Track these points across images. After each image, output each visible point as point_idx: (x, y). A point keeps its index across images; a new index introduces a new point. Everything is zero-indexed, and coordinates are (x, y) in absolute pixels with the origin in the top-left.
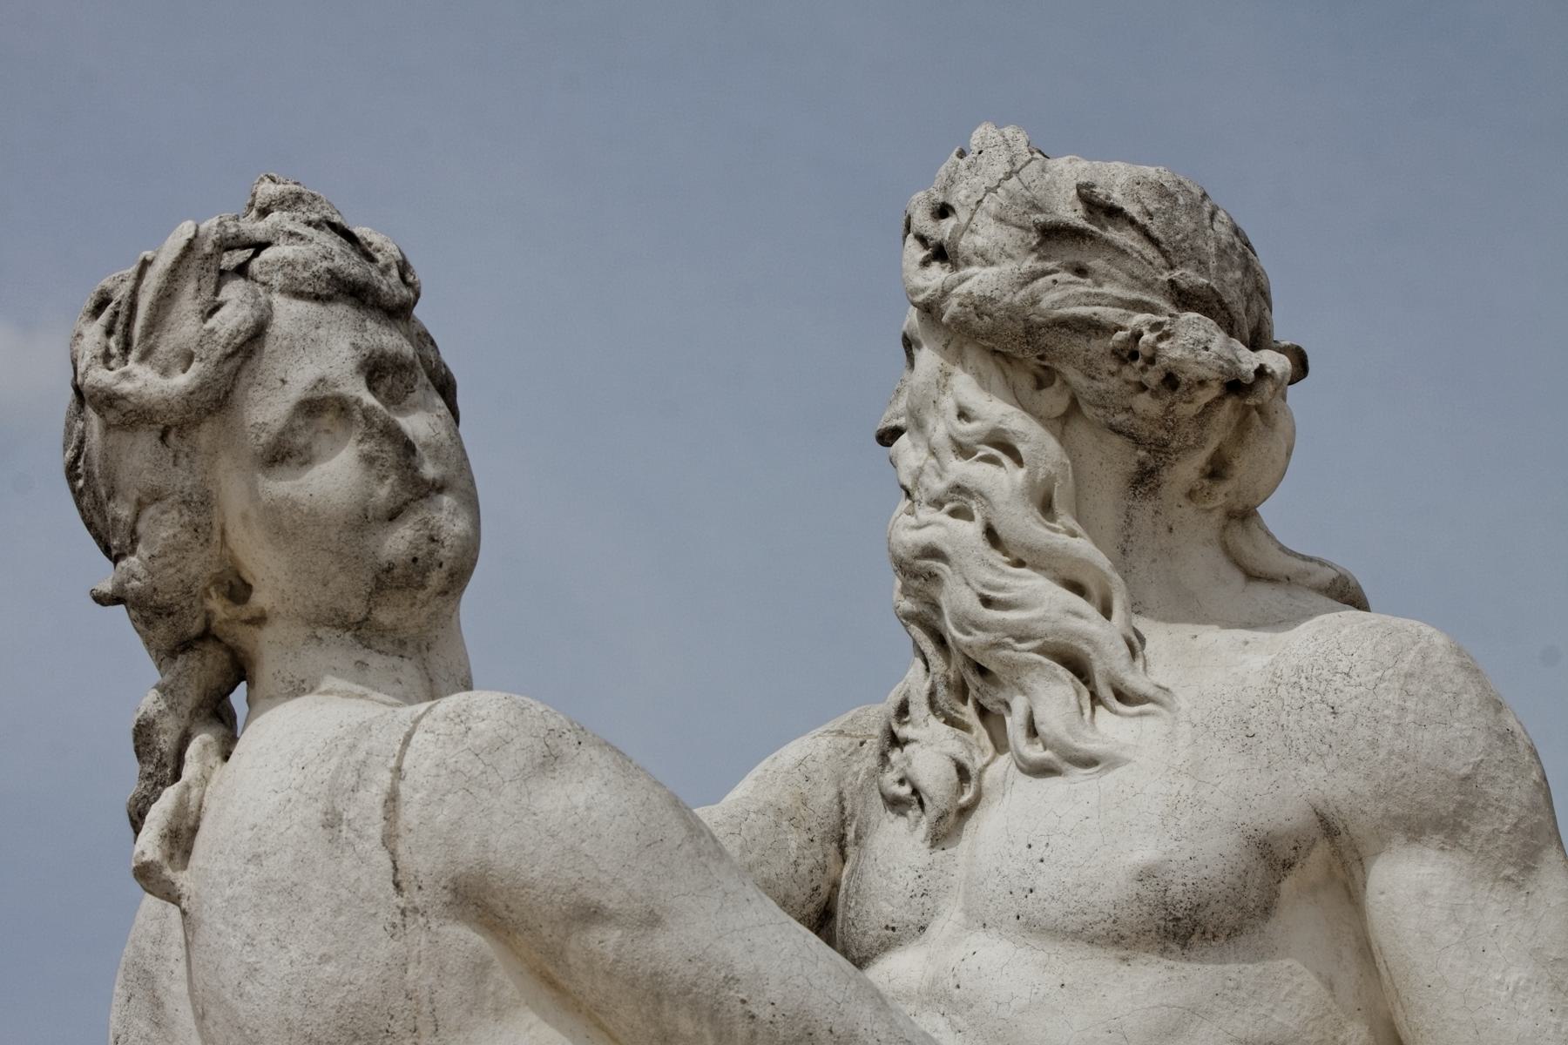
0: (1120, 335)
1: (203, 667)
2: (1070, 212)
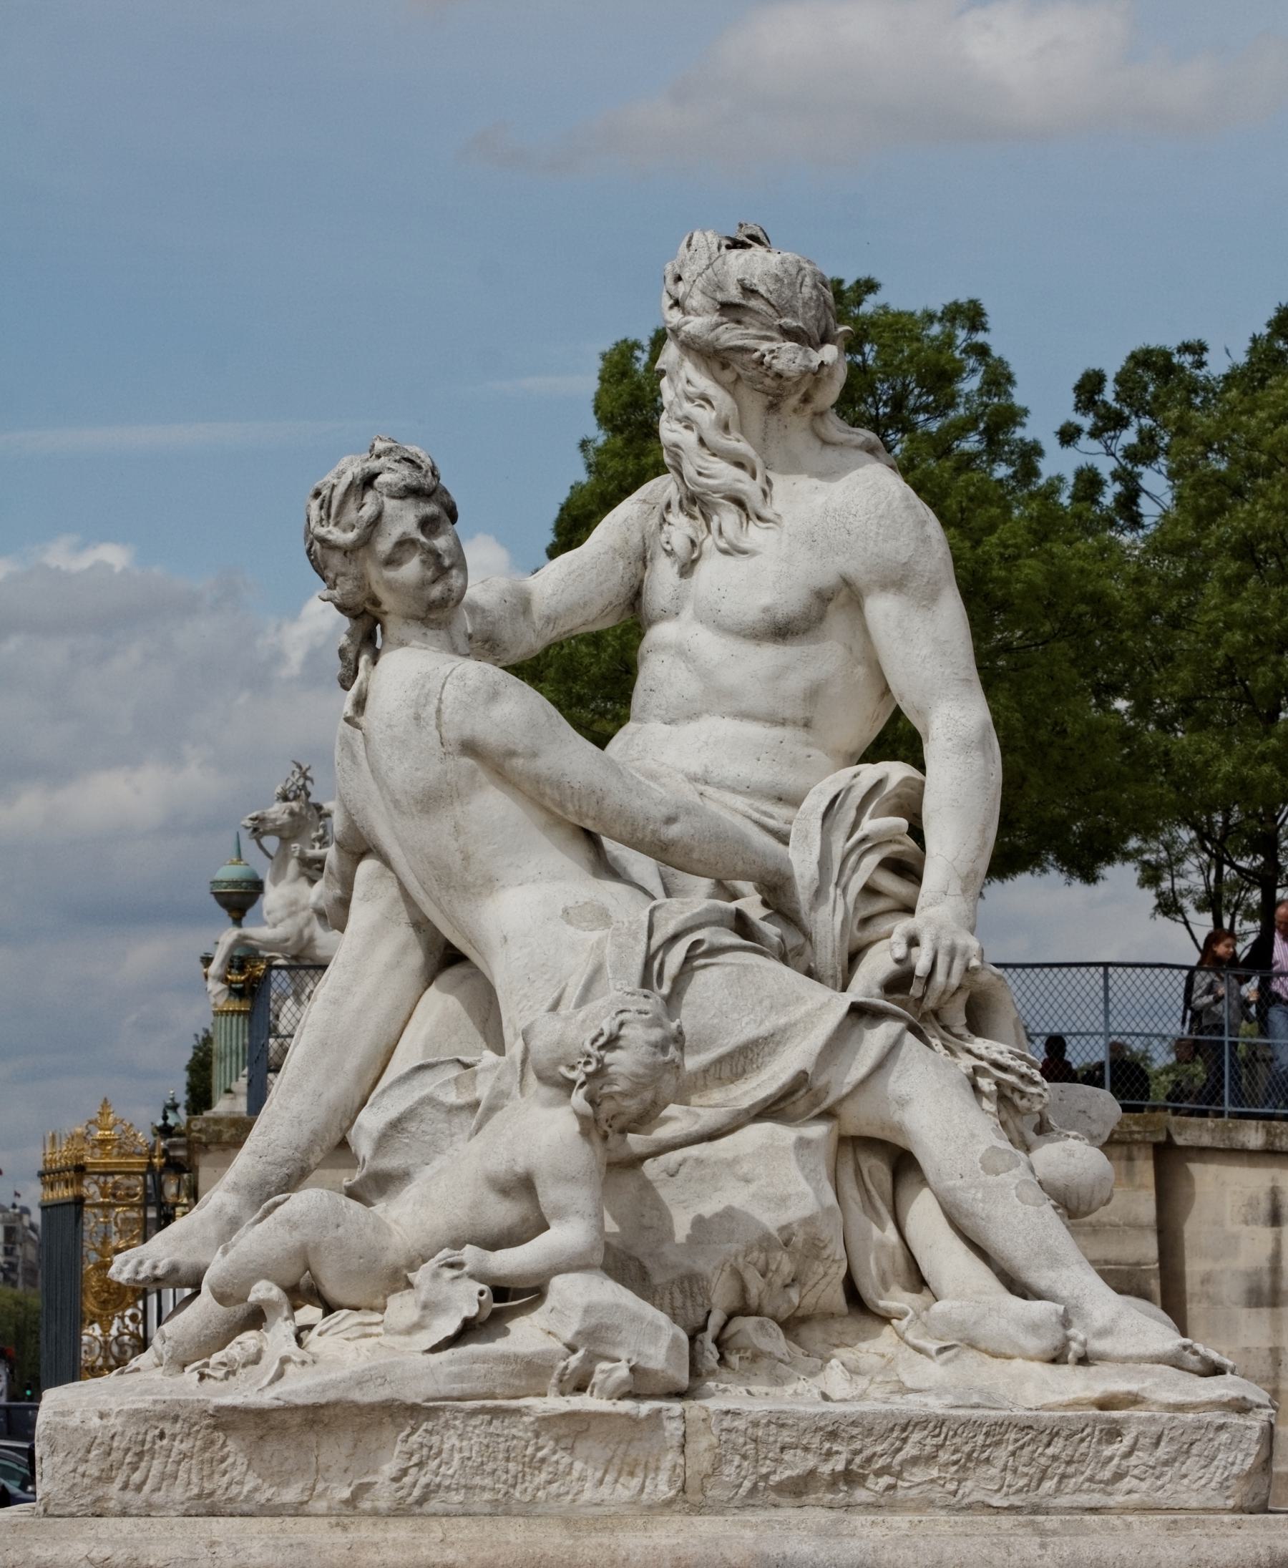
1: (364, 624)
2: (734, 294)
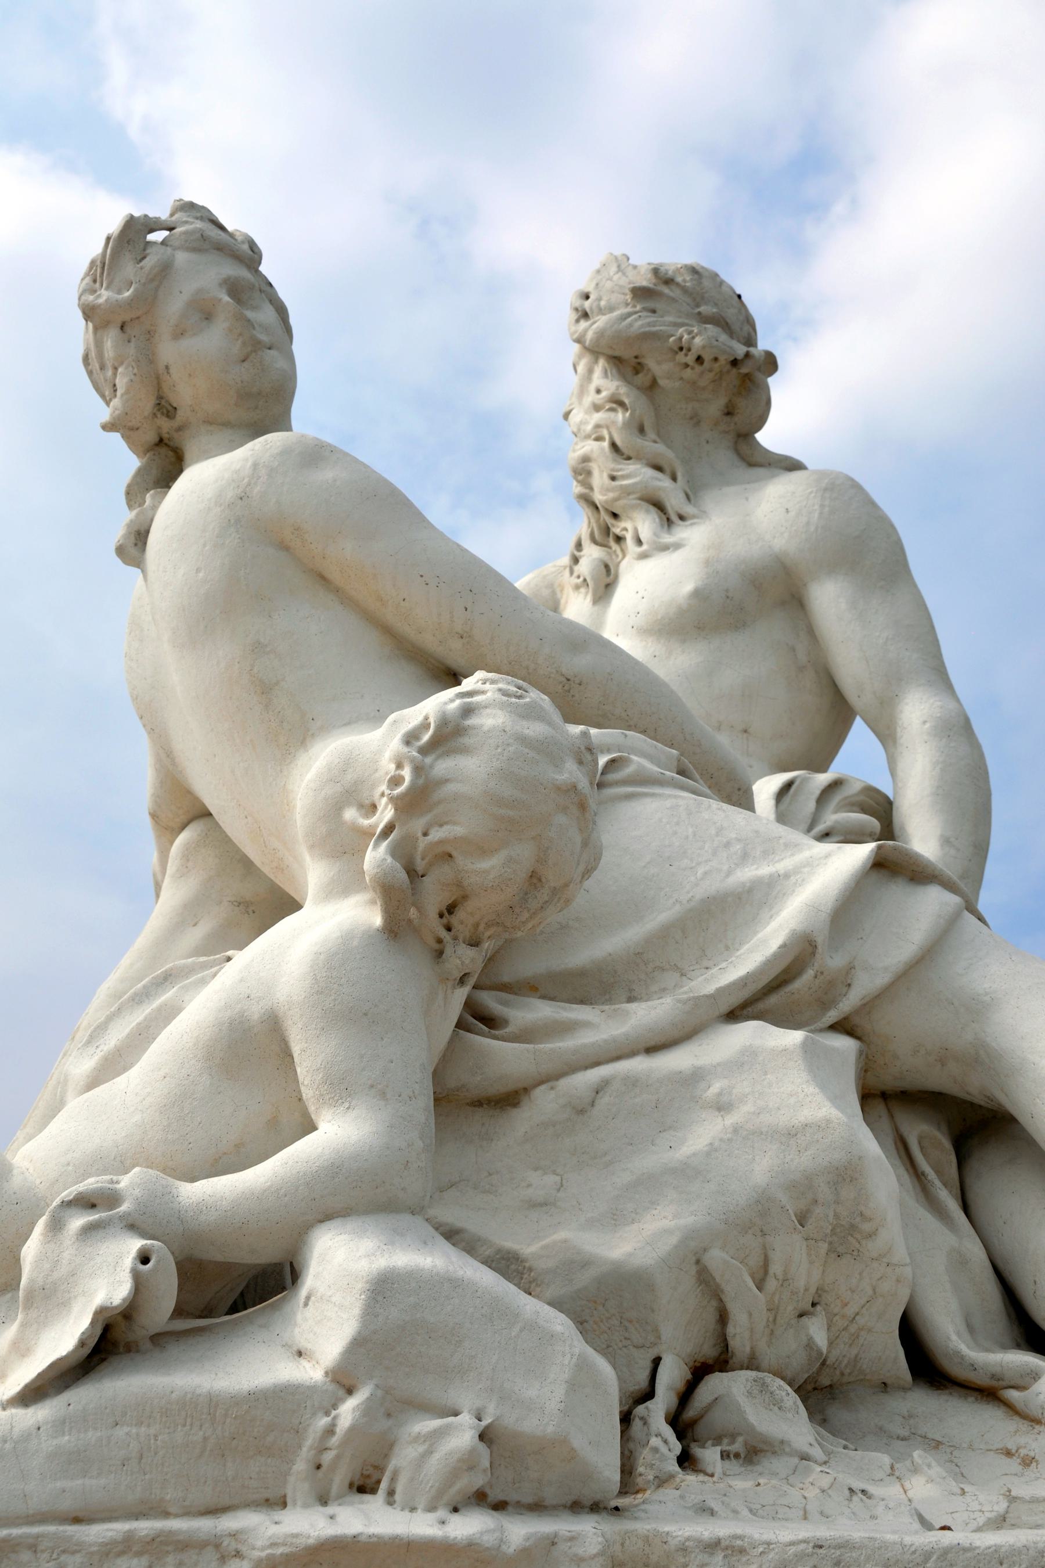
0: (672, 339)
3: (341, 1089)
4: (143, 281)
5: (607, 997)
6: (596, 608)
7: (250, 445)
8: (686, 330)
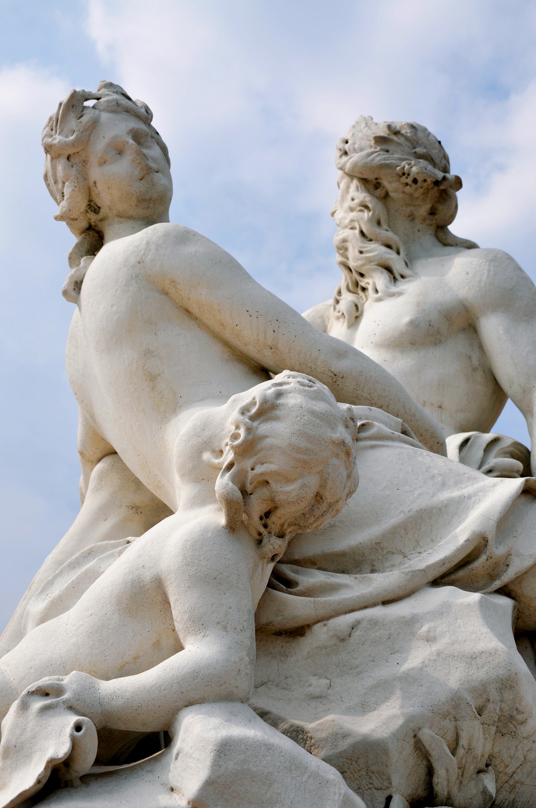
0: (398, 168)
3: (200, 624)
4: (81, 130)
5: (358, 569)
6: (350, 331)
7: (145, 230)
8: (407, 163)
